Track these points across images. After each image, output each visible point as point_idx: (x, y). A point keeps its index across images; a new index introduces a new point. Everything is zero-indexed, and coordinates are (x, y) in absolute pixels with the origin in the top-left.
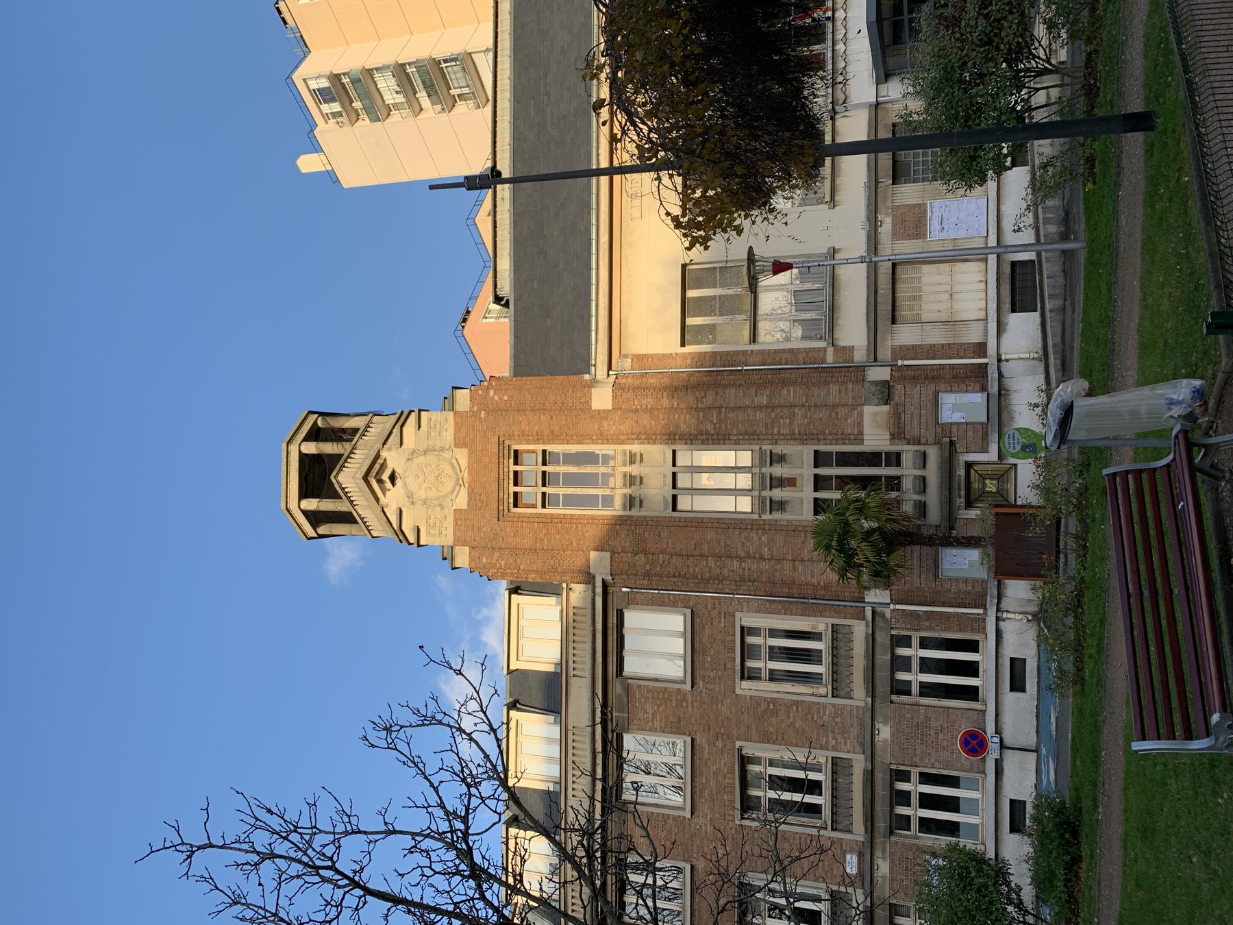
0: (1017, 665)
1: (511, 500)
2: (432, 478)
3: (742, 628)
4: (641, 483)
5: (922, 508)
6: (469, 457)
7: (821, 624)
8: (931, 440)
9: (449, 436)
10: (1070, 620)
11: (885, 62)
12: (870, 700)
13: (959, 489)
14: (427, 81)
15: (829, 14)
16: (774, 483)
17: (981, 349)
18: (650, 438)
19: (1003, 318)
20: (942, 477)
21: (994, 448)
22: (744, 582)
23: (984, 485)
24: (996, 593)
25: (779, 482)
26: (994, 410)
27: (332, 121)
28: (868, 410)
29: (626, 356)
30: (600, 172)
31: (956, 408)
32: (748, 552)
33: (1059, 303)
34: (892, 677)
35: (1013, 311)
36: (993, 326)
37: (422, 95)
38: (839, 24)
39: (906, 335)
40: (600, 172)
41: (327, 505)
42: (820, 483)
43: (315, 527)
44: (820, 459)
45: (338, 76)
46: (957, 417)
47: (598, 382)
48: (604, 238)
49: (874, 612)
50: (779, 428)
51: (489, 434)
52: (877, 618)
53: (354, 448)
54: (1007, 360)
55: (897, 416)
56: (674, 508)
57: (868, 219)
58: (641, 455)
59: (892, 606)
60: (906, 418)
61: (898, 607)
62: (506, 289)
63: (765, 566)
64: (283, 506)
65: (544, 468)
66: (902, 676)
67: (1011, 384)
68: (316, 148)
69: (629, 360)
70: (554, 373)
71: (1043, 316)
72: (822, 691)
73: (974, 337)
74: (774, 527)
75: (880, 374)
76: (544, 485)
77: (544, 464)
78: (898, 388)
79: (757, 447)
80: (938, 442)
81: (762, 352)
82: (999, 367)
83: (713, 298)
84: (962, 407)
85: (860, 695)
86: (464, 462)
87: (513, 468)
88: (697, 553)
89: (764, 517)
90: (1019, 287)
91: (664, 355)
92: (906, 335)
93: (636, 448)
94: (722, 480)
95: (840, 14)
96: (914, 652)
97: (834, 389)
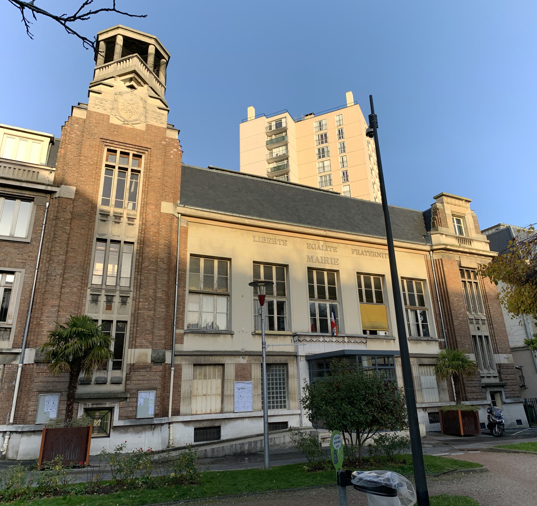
1: (112, 148)
2: (130, 107)
4: (116, 222)
5: (87, 382)
8: (128, 387)
9: (153, 122)
10: (35, 485)
15: (335, 334)
16: (110, 298)
17: (176, 413)
18: (143, 230)
20: (105, 394)
21: (121, 423)
25: (109, 300)
28: (149, 351)
29: (187, 224)
31: (146, 400)
32: (67, 279)
35: (195, 429)
37: (275, 165)
38: (331, 338)
39: (187, 371)
42: (107, 323)
45: (286, 131)
46: (141, 401)
47: (176, 207)
50: (143, 302)
51: (152, 144)
53: (150, 72)
54: (169, 427)
55: (145, 367)
56: (99, 240)
58: (132, 225)
59: (21, 365)
60: (143, 372)
61: (20, 369)
63: (57, 289)
64: (121, 26)
65: (129, 170)
67: (157, 431)
68: (257, 116)
69: (185, 226)
73: (183, 409)
74: (81, 297)
77: (132, 170)
78: (160, 368)
79: (132, 289)
81: (184, 296)
82: (167, 423)
84: (147, 403)
86: (137, 127)
88: (69, 249)
89: (89, 290)
90: (208, 431)
92: (187, 371)
93: (137, 222)
95: (334, 339)
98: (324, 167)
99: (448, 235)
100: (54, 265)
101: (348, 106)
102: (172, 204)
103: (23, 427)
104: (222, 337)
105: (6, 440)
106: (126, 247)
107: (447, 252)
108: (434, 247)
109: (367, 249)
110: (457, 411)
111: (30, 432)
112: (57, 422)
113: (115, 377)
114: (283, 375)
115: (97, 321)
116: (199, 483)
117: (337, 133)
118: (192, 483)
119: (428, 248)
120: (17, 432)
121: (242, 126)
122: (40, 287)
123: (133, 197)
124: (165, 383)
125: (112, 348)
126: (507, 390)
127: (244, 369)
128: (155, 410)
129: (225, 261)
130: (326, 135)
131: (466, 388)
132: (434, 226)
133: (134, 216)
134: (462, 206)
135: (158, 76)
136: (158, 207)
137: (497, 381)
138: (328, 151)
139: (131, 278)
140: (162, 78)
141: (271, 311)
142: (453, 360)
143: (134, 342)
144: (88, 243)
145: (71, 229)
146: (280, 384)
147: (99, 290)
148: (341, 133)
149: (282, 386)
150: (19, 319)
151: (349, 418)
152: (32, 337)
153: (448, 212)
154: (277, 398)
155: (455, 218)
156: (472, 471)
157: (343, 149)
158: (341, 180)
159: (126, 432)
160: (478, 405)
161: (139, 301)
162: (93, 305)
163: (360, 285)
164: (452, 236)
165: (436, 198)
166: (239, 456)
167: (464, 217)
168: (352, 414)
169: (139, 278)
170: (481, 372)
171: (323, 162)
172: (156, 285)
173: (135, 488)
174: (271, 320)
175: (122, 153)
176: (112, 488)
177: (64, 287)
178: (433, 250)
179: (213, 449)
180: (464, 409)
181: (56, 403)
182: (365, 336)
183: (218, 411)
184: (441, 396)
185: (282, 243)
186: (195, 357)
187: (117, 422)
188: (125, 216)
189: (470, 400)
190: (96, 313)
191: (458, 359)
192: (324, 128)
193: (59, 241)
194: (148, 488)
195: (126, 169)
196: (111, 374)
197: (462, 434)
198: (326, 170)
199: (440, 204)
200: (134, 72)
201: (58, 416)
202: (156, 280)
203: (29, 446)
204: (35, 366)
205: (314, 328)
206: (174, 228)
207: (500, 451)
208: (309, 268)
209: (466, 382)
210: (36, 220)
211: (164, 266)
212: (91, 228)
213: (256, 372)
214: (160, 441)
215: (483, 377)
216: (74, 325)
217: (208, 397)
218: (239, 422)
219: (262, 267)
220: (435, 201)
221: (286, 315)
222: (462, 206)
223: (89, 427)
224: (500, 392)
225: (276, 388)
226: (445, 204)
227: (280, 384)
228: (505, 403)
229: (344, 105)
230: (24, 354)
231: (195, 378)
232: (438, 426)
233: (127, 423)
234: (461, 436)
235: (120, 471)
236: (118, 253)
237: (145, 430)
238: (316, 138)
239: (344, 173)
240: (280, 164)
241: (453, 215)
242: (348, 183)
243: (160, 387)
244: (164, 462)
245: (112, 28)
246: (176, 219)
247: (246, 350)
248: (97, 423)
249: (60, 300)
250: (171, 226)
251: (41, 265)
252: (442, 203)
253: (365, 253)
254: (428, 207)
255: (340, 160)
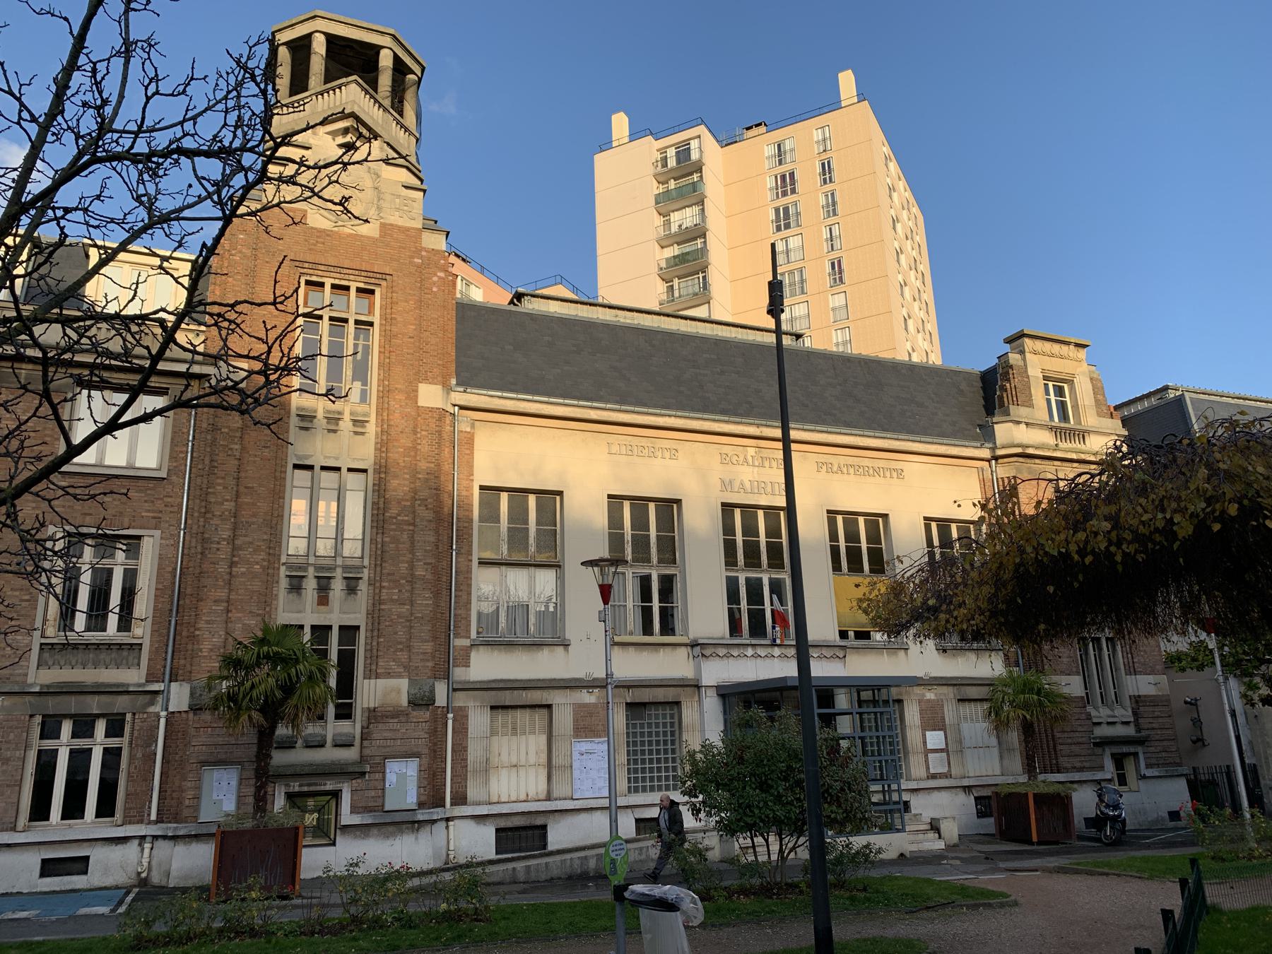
0: (80, 865)
1: (314, 279)
3: (139, 538)
4: (329, 431)
5: (288, 745)
6: (368, 238)
7: (141, 632)
8: (367, 752)
10: (218, 924)
11: (734, 694)
12: (37, 689)
13: (309, 785)
14: (689, 257)
15: (778, 642)
16: (324, 582)
17: (460, 799)
18: (383, 445)
19: (491, 820)
20: (324, 765)
21: (356, 820)
22: (201, 541)
23: (312, 812)
24: (181, 833)
25: (324, 586)
26: (398, 817)
27: (659, 157)
28: (403, 684)
29: (473, 426)
30: (786, 430)
31: (402, 777)
33: (521, 876)
34: (65, 716)
35: (497, 830)
36: (483, 810)
37: (675, 251)
38: (770, 650)
39: (479, 720)
40: (786, 430)
41: (317, 64)
42: (321, 632)
43: (288, 44)
44: (349, 632)
45: (700, 170)
46: (391, 778)
48: (594, 415)
49: (156, 692)
50: (389, 588)
51: (395, 264)
52: (148, 697)
53: (385, 110)
54: (447, 827)
55: (396, 714)
56: (296, 467)
57: (595, 679)
58: (363, 434)
59: (163, 714)
60: (393, 724)
61: (163, 721)
62: (530, 305)
63: (222, 568)
65: (351, 322)
66: (67, 728)
67: (424, 834)
68: (634, 135)
69: (468, 429)
70: (458, 349)
71: (491, 862)
72: (50, 631)
73: (472, 792)
74: (270, 581)
75: (441, 691)
76: (331, 319)
77: (357, 322)
78: (425, 715)
79: (366, 562)
80: (363, 759)
81: (469, 571)
82: (441, 819)
83: (526, 522)
84: (402, 781)
85: (39, 676)
87: (353, 286)
88: (242, 489)
89: (283, 569)
90: (522, 835)
91: (471, 467)
92: (479, 720)
93: (372, 428)
94: (324, 520)
95: (777, 651)
96: (99, 740)
97: (428, 647)
98: (787, 252)
99: (1032, 424)
100: (215, 521)
101: (843, 104)
102: (440, 387)
103: (176, 829)
104: (546, 651)
105: (147, 851)
106: (353, 480)
107: (1028, 460)
108: (999, 452)
109: (850, 461)
110: (1026, 795)
111: (189, 836)
112: (239, 817)
113: (340, 735)
114: (672, 724)
115: (302, 627)
116: (488, 920)
117: (819, 169)
118: (476, 920)
119: (986, 453)
120: (165, 837)
121: (601, 160)
122: (191, 564)
123: (361, 373)
124: (435, 744)
125: (333, 683)
126: (1152, 749)
127: (591, 715)
128: (419, 795)
129: (550, 498)
130: (792, 175)
131: (1059, 747)
132: (1002, 405)
133: (365, 415)
134: (1068, 358)
135: (401, 115)
136: (413, 395)
137: (1130, 731)
138: (798, 214)
139: (363, 539)
140: (410, 118)
141: (646, 595)
142: (1023, 692)
143: (374, 667)
144: (278, 474)
145: (243, 449)
146: (665, 742)
147: (303, 568)
148: (826, 170)
149: (669, 747)
150: (156, 627)
151: (757, 811)
152: (182, 662)
153: (1035, 372)
154: (659, 770)
155: (1050, 384)
156: (984, 905)
157: (832, 208)
158: (828, 281)
159: (366, 836)
160: (1072, 782)
161: (381, 587)
162: (293, 596)
163: (833, 536)
164: (1041, 426)
165: (1009, 341)
166: (579, 879)
167: (1070, 382)
168: (761, 804)
169: (379, 540)
170: (1094, 713)
171: (786, 239)
172: (413, 554)
173: (381, 927)
174: (647, 613)
175: (334, 286)
176: (343, 928)
177: (237, 563)
178: (996, 458)
179: (529, 867)
180: (1043, 789)
181: (234, 783)
182: (843, 643)
183: (543, 796)
184: (1006, 762)
185: (667, 455)
186: (493, 693)
187: (347, 818)
188: (347, 416)
189: (1067, 770)
190: (300, 612)
191: (1031, 691)
192: (788, 160)
193: (223, 474)
194: (403, 927)
195: (346, 321)
196: (333, 727)
197: (1035, 839)
198: (792, 258)
199: (1018, 356)
200: (353, 115)
201: (238, 808)
202: (412, 543)
203: (192, 862)
204: (191, 715)
205: (735, 627)
206: (445, 436)
207: (1077, 872)
208: (723, 504)
209: (1058, 735)
210: (174, 432)
211: (428, 515)
212: (283, 442)
213: (619, 719)
214: (430, 852)
215: (1099, 724)
216: (262, 642)
217: (522, 772)
218: (583, 816)
219: (627, 505)
220: (1007, 347)
221: (678, 603)
222: (1068, 358)
223: (297, 828)
224: (1136, 755)
225: (658, 752)
226: (1028, 355)
227: (665, 742)
228: (1144, 777)
229: (834, 104)
230: (169, 692)
231: (493, 732)
232: (989, 824)
233: (368, 819)
234: (1033, 844)
235: (354, 901)
236: (336, 492)
237: (402, 832)
238: (770, 182)
239: (833, 264)
240: (687, 248)
241: (1045, 378)
242: (842, 288)
243: (426, 751)
244: (435, 891)
245: (303, 18)
246: (448, 419)
247: (595, 676)
248: (311, 819)
249: (230, 590)
250: (440, 433)
251: (189, 522)
252: (1022, 352)
253: (845, 470)
254: (993, 362)
255: (826, 234)
